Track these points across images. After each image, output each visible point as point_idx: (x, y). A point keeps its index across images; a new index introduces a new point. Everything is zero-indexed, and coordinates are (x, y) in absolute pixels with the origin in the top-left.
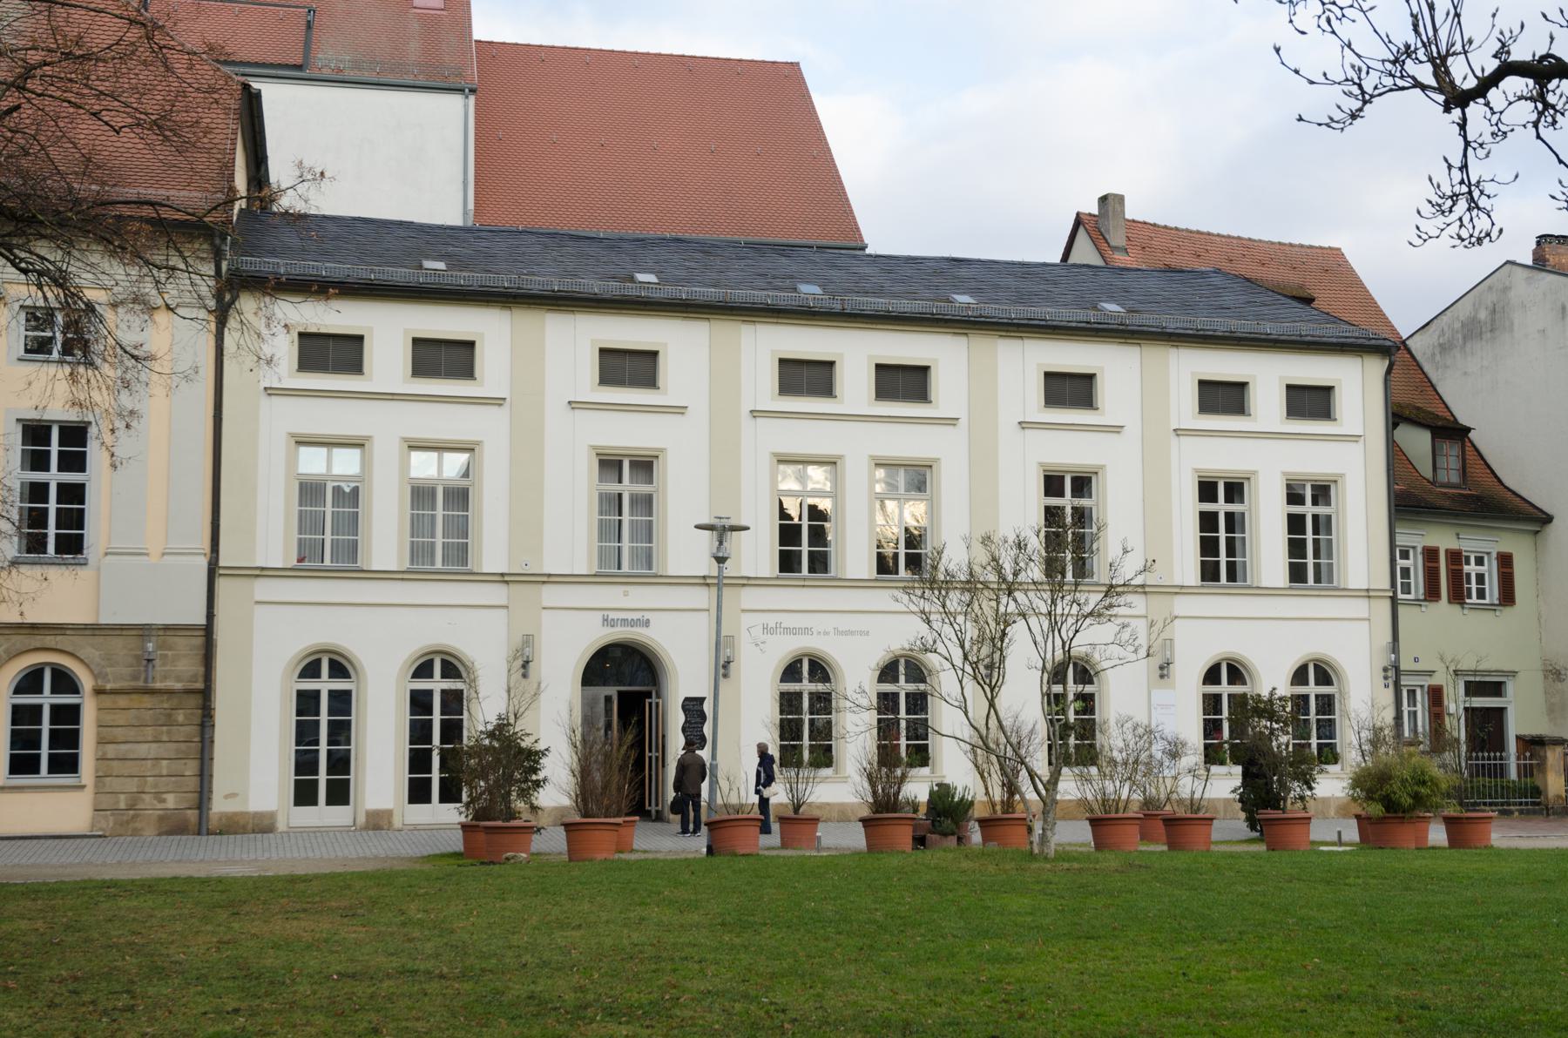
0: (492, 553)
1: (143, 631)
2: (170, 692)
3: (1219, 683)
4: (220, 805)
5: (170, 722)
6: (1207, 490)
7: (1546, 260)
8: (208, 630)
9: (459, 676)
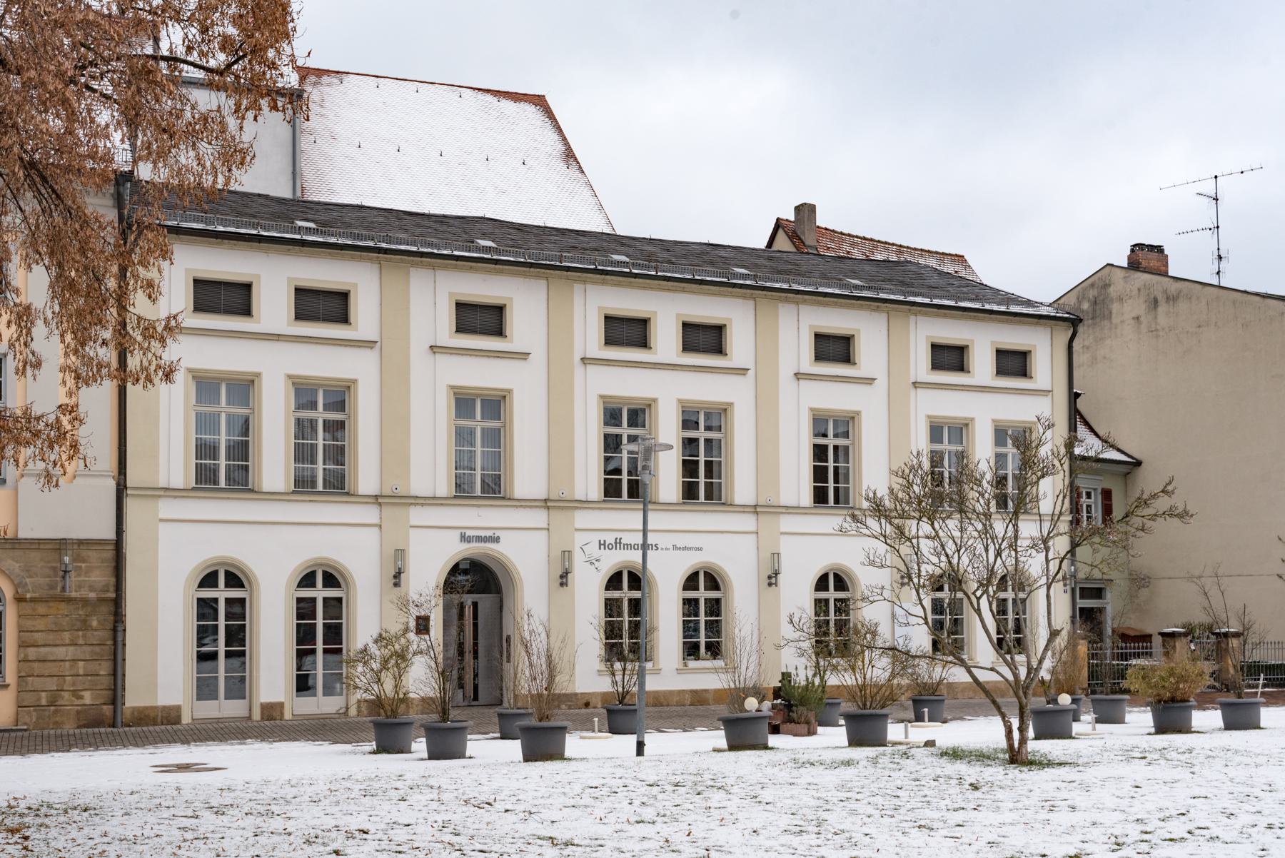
0: (366, 477)
1: (60, 545)
2: (85, 602)
3: (620, 588)
4: (134, 699)
5: (85, 625)
6: (612, 416)
7: (1139, 263)
8: (118, 545)
9: (242, 586)
